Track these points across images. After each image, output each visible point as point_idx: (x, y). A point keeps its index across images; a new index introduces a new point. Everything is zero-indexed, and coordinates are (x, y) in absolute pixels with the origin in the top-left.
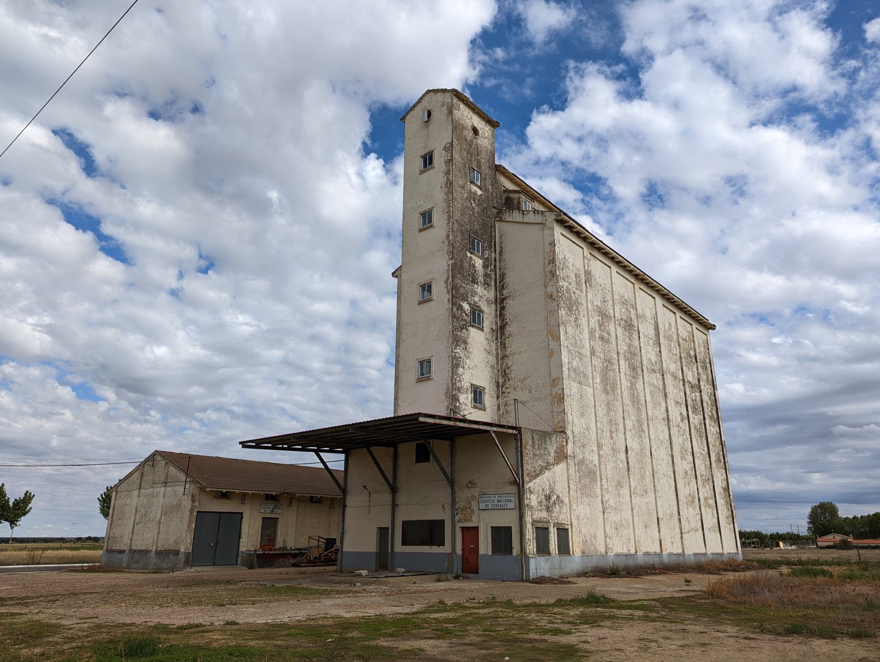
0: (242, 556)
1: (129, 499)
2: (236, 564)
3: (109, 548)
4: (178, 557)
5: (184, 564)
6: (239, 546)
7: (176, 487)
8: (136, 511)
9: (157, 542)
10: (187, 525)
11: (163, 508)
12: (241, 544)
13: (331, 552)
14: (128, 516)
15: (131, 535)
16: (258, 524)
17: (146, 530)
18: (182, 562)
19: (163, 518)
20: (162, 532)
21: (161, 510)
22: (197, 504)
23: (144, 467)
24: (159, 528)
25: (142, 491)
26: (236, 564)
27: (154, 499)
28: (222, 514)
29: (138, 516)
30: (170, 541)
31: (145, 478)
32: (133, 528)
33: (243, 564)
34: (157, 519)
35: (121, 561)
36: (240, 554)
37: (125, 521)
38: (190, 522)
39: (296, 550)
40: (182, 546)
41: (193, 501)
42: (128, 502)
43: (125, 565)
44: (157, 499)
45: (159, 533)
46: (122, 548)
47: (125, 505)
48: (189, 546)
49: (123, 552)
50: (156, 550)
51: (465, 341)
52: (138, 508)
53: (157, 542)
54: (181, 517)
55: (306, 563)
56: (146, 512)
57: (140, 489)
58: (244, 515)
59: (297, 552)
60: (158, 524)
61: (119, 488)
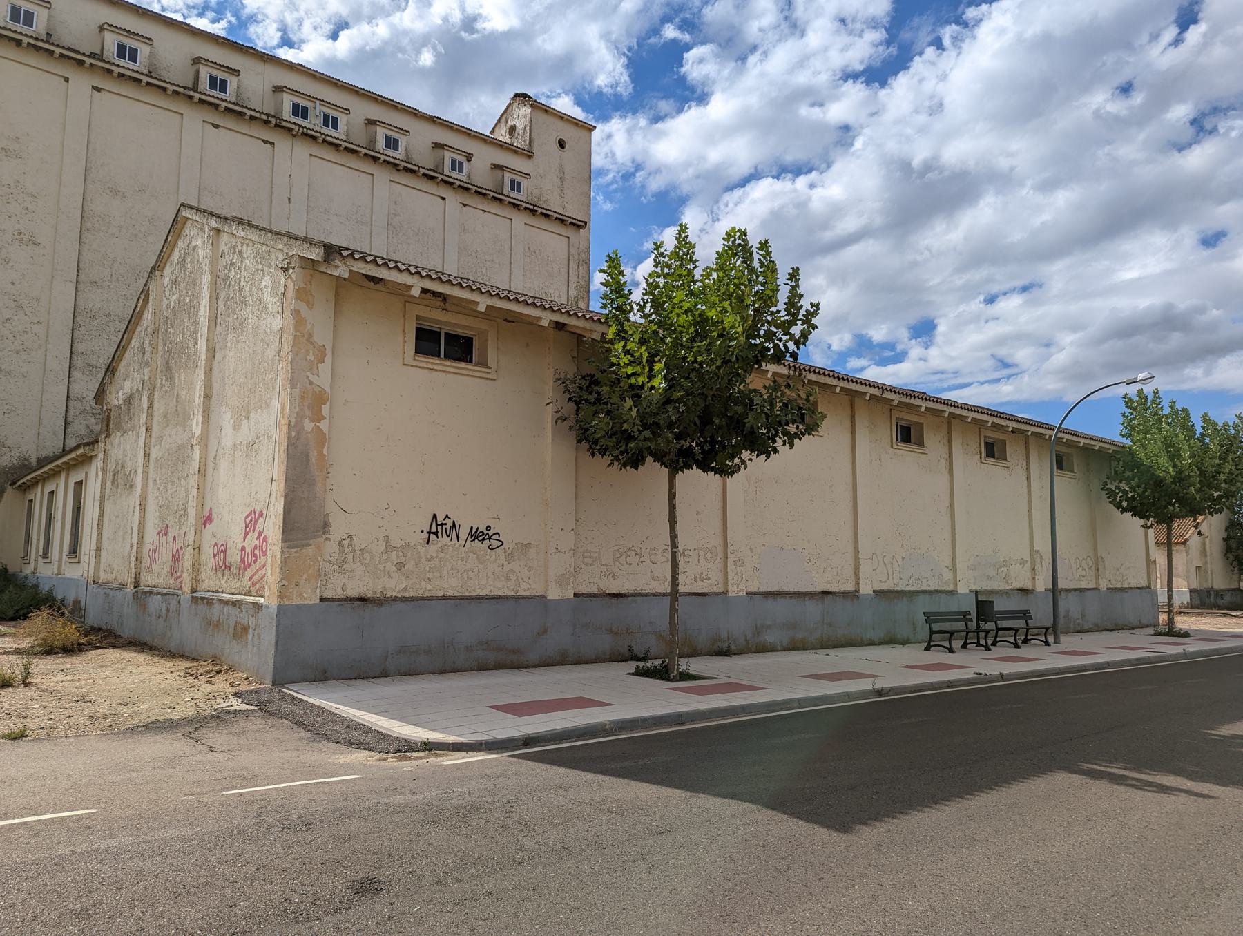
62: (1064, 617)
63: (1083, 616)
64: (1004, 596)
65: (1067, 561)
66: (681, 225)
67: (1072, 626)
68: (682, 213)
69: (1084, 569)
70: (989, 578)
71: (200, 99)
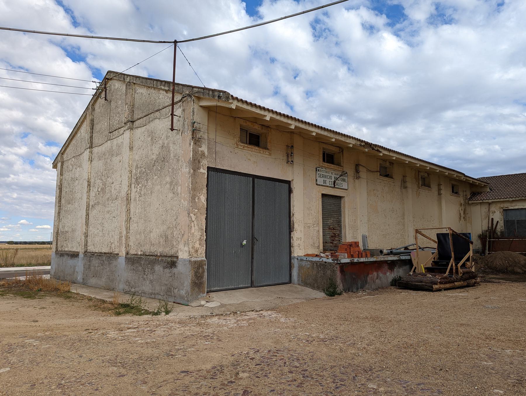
0: (300, 267)
1: (78, 169)
2: (290, 282)
3: (59, 249)
4: (175, 270)
5: (193, 289)
6: (290, 246)
7: (152, 125)
8: (89, 185)
9: (127, 237)
10: (186, 195)
11: (131, 172)
12: (295, 242)
13: (468, 260)
14: (78, 196)
15: (84, 227)
16: (317, 205)
17: (107, 216)
18: (187, 283)
19: (134, 190)
20: (134, 219)
21: (128, 174)
22: (204, 148)
23: (93, 109)
24: (128, 211)
25: (95, 150)
26: (290, 282)
27: (114, 159)
28: (256, 180)
29: (92, 194)
30: (154, 236)
31: (97, 127)
32: (88, 215)
33: (305, 283)
34: (123, 194)
35: (74, 271)
36: (295, 263)
37: (76, 204)
38: (194, 190)
39: (391, 253)
40: (181, 246)
41: (197, 141)
42: (77, 175)
43: (80, 278)
44: (118, 158)
45: (129, 220)
46: (74, 250)
47: (74, 180)
48: (197, 245)
49: (74, 255)
50: (127, 253)
51: (133, 264)
52: (92, 181)
53: (127, 237)
54: (171, 183)
55: (441, 283)
56: (104, 184)
57: (91, 147)
58: (294, 186)
59: (395, 258)
60: (125, 203)
61: (65, 156)
62: (481, 255)
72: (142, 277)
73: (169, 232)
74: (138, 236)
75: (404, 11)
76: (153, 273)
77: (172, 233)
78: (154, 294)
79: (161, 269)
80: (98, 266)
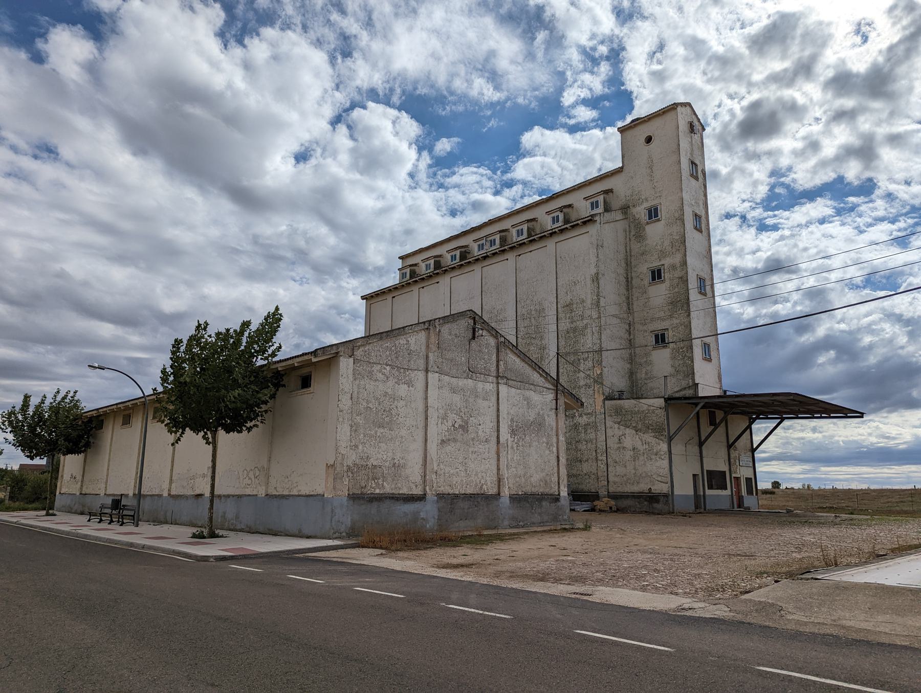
62: (222, 517)
63: (237, 517)
64: (185, 499)
65: (236, 473)
66: (315, 142)
67: (226, 524)
68: (473, 97)
69: (250, 479)
70: (183, 487)
71: (582, 222)
72: (531, 512)
73: (548, 478)
74: (518, 479)
75: (227, 19)
76: (541, 507)
77: (550, 479)
78: (543, 522)
79: (548, 504)
80: (469, 508)
